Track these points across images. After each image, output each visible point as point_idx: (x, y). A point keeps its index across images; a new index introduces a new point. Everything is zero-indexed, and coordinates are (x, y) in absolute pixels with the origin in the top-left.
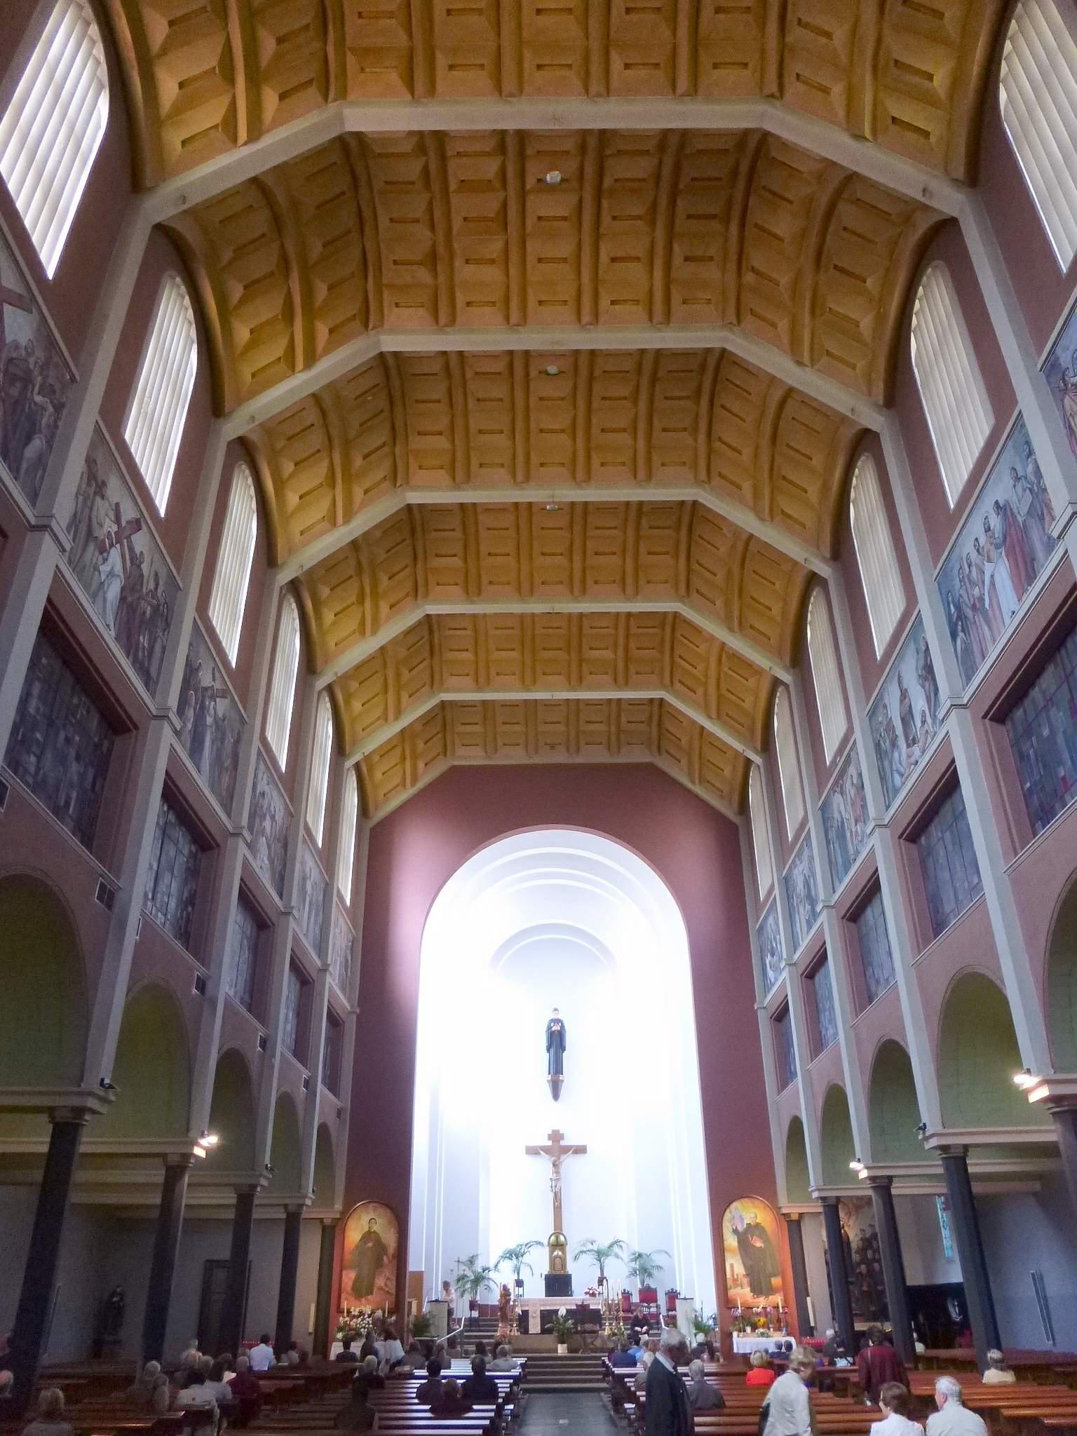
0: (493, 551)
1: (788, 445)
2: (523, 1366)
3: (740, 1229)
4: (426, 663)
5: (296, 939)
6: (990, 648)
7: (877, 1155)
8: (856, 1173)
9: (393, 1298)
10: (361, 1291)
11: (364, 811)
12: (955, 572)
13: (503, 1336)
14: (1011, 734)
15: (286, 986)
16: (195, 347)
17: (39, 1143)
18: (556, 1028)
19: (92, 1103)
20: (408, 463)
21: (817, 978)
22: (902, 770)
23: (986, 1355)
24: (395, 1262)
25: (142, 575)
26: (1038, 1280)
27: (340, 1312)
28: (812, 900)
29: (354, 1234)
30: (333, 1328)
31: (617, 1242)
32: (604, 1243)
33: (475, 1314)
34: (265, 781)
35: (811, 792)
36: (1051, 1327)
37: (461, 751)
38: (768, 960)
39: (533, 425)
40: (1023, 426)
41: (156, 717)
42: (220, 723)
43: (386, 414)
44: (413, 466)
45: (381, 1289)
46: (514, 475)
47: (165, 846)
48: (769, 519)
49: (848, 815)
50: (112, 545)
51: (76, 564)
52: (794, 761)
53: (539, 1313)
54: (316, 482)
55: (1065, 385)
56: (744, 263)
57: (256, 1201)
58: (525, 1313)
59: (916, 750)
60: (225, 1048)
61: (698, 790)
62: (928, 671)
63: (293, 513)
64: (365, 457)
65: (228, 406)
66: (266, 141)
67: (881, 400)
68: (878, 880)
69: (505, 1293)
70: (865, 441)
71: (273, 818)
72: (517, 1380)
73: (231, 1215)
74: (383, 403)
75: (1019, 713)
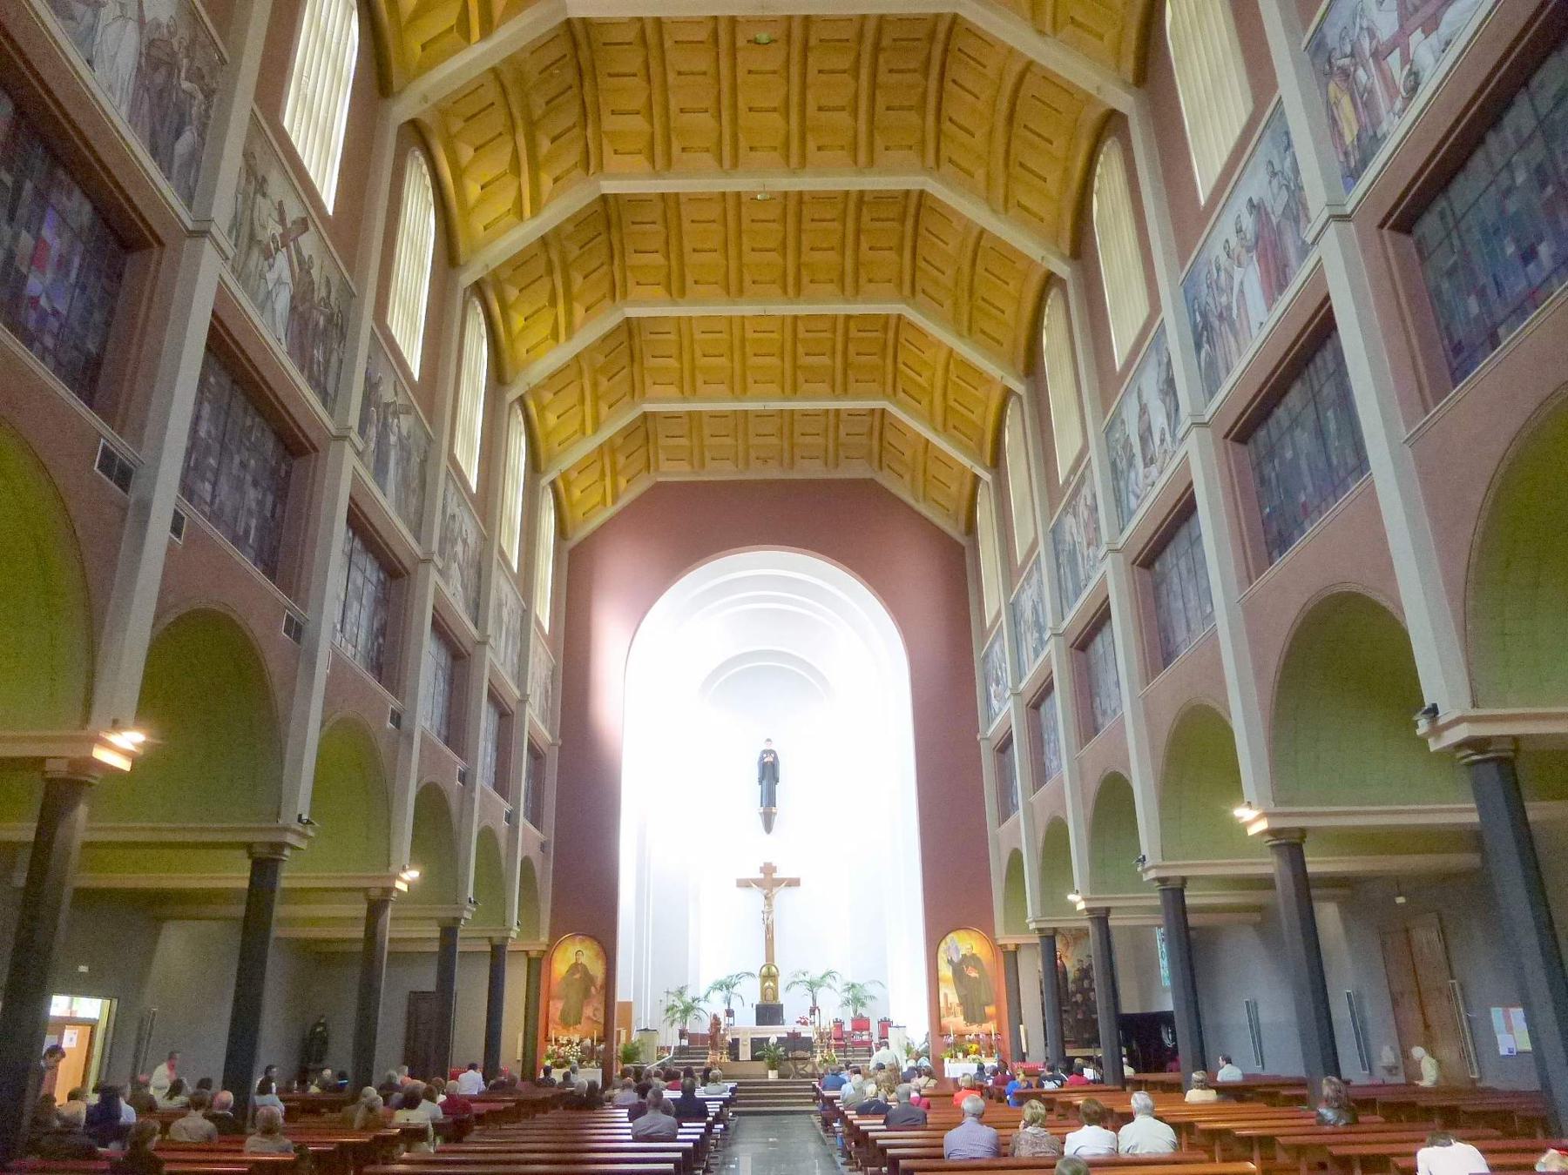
0: (699, 246)
1: (1025, 126)
3: (955, 959)
5: (492, 666)
6: (1236, 363)
7: (1098, 881)
8: (1073, 905)
9: (601, 1028)
10: (567, 1022)
12: (1203, 276)
14: (1253, 456)
15: (485, 722)
17: (237, 876)
18: (769, 759)
19: (291, 839)
20: (601, 145)
21: (1042, 709)
22: (1138, 491)
24: (603, 992)
25: (312, 283)
26: (1252, 1007)
27: (548, 1040)
28: (1040, 629)
29: (562, 962)
31: (829, 974)
32: (816, 973)
33: (685, 1042)
36: (1261, 1053)
37: (665, 466)
38: (993, 689)
39: (741, 105)
40: (1283, 114)
41: (193, 234)
42: (405, 442)
43: (575, 90)
45: (589, 1018)
46: (720, 161)
49: (1081, 539)
50: (277, 249)
51: (241, 274)
52: (1025, 474)
55: (1331, 67)
58: (736, 1042)
59: (1154, 469)
60: (425, 781)
61: (921, 507)
62: (1169, 387)
64: (553, 140)
65: (396, 83)
69: (716, 1022)
70: (1112, 123)
71: (465, 542)
72: (727, 1103)
73: (435, 947)
74: (570, 76)
75: (1262, 434)
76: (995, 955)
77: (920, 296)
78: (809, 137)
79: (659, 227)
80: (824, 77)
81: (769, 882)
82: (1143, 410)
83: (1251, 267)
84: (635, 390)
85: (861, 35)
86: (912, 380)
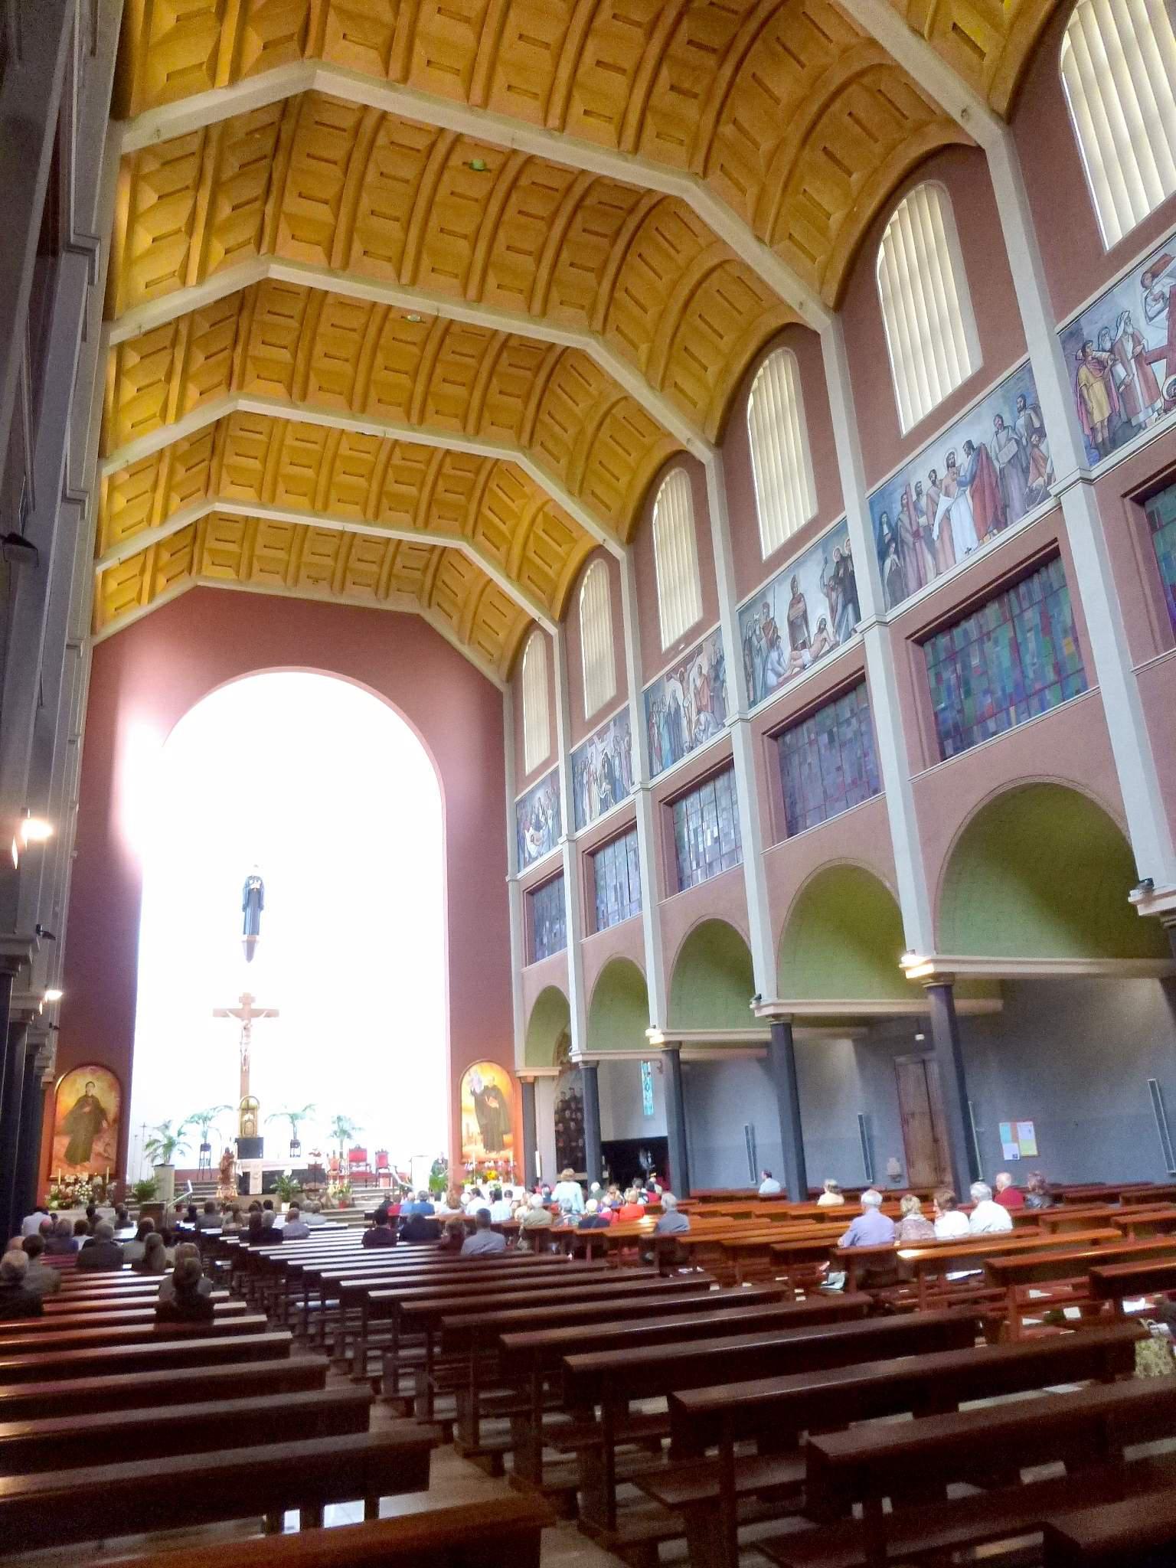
0: (333, 352)
3: (478, 1091)
9: (113, 1164)
10: (74, 1158)
12: (897, 496)
18: (256, 885)
26: (750, 1132)
37: (209, 570)
45: (99, 1154)
48: (658, 388)
53: (261, 1174)
56: (726, 111)
59: (806, 655)
61: (465, 650)
63: (142, 257)
76: (514, 1085)
77: (538, 448)
78: (490, 273)
79: (294, 324)
80: (523, 219)
81: (247, 1012)
82: (797, 599)
83: (961, 500)
84: (210, 486)
85: (569, 188)
86: (496, 528)
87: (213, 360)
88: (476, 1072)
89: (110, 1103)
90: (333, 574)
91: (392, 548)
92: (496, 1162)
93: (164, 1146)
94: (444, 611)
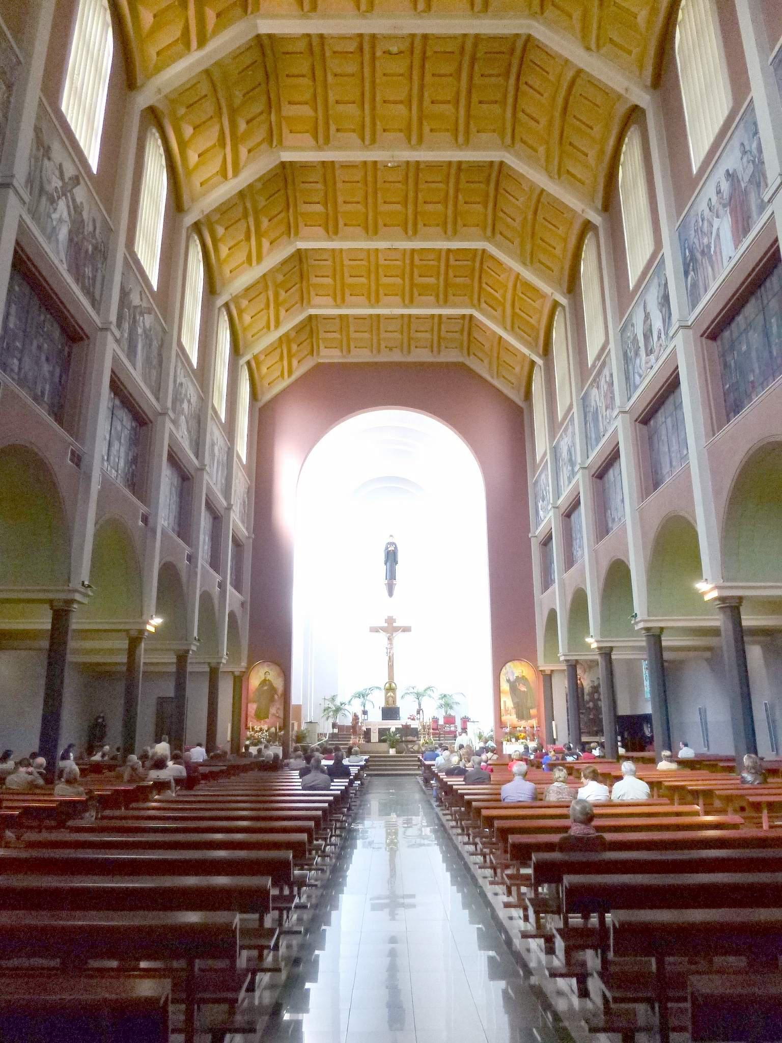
2: (366, 760)
3: (512, 679)
4: (298, 286)
5: (209, 488)
7: (605, 631)
9: (282, 721)
10: (261, 715)
11: (254, 396)
12: (693, 222)
13: (354, 744)
14: (720, 349)
15: (204, 522)
16: (165, 170)
17: (44, 623)
18: (391, 548)
19: (78, 597)
22: (641, 372)
23: (661, 754)
25: (83, 221)
26: (702, 712)
27: (247, 728)
28: (572, 463)
29: (255, 681)
30: (242, 738)
32: (421, 689)
33: (336, 731)
34: (182, 375)
35: (577, 384)
36: (771, 739)
40: (753, 110)
41: (102, 329)
42: (147, 332)
44: (312, 293)
45: (273, 715)
47: (114, 423)
49: (602, 404)
50: (59, 198)
51: (34, 213)
54: (209, 144)
57: (189, 661)
59: (652, 357)
60: (163, 562)
61: (496, 382)
66: (212, 45)
67: (649, 82)
68: (618, 450)
69: (356, 718)
70: (634, 114)
71: (189, 401)
72: (363, 768)
73: (173, 669)
74: (260, 76)
75: (726, 334)
76: (538, 677)
77: (498, 236)
79: (320, 186)
81: (391, 628)
85: (463, 48)
87: (275, 220)
88: (510, 667)
89: (279, 684)
90: (402, 343)
91: (436, 320)
92: (524, 728)
93: (333, 711)
94: (478, 358)
